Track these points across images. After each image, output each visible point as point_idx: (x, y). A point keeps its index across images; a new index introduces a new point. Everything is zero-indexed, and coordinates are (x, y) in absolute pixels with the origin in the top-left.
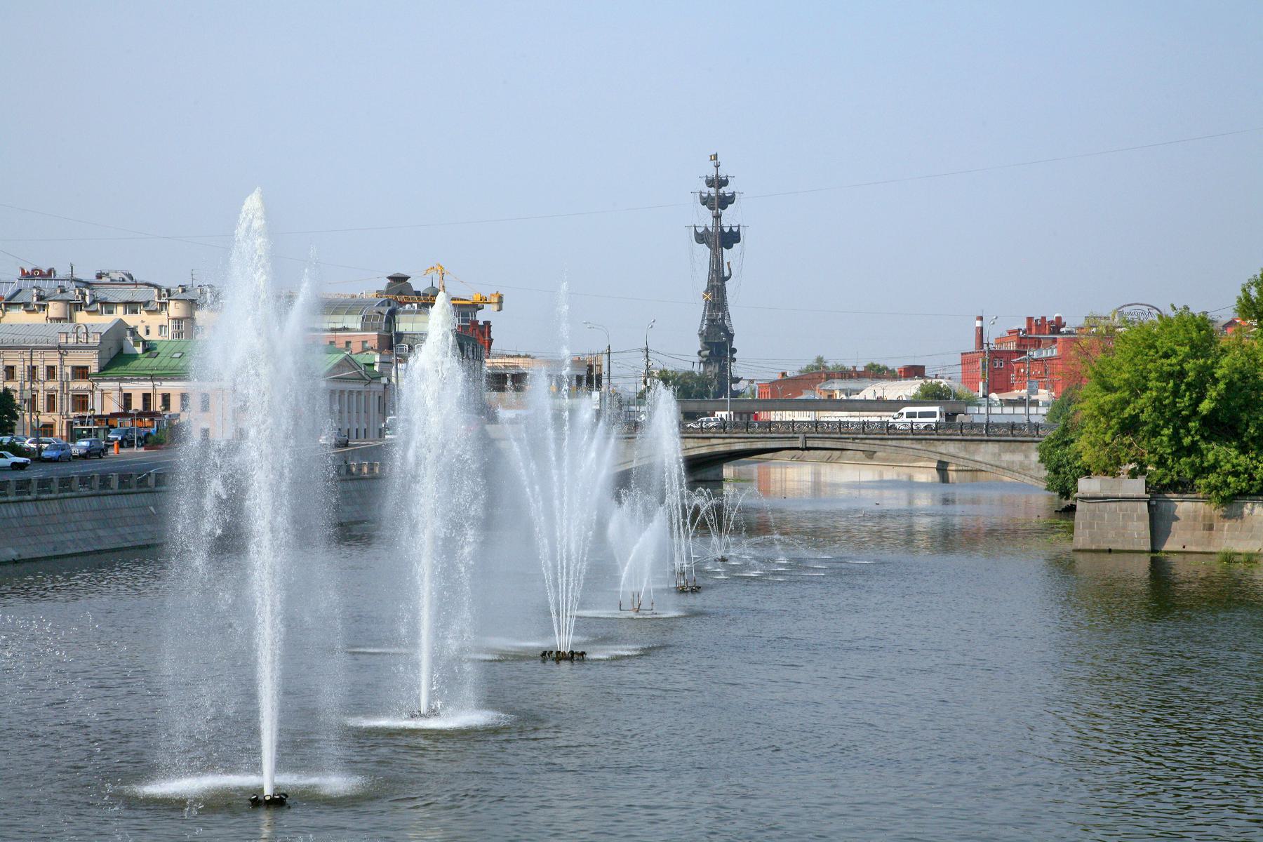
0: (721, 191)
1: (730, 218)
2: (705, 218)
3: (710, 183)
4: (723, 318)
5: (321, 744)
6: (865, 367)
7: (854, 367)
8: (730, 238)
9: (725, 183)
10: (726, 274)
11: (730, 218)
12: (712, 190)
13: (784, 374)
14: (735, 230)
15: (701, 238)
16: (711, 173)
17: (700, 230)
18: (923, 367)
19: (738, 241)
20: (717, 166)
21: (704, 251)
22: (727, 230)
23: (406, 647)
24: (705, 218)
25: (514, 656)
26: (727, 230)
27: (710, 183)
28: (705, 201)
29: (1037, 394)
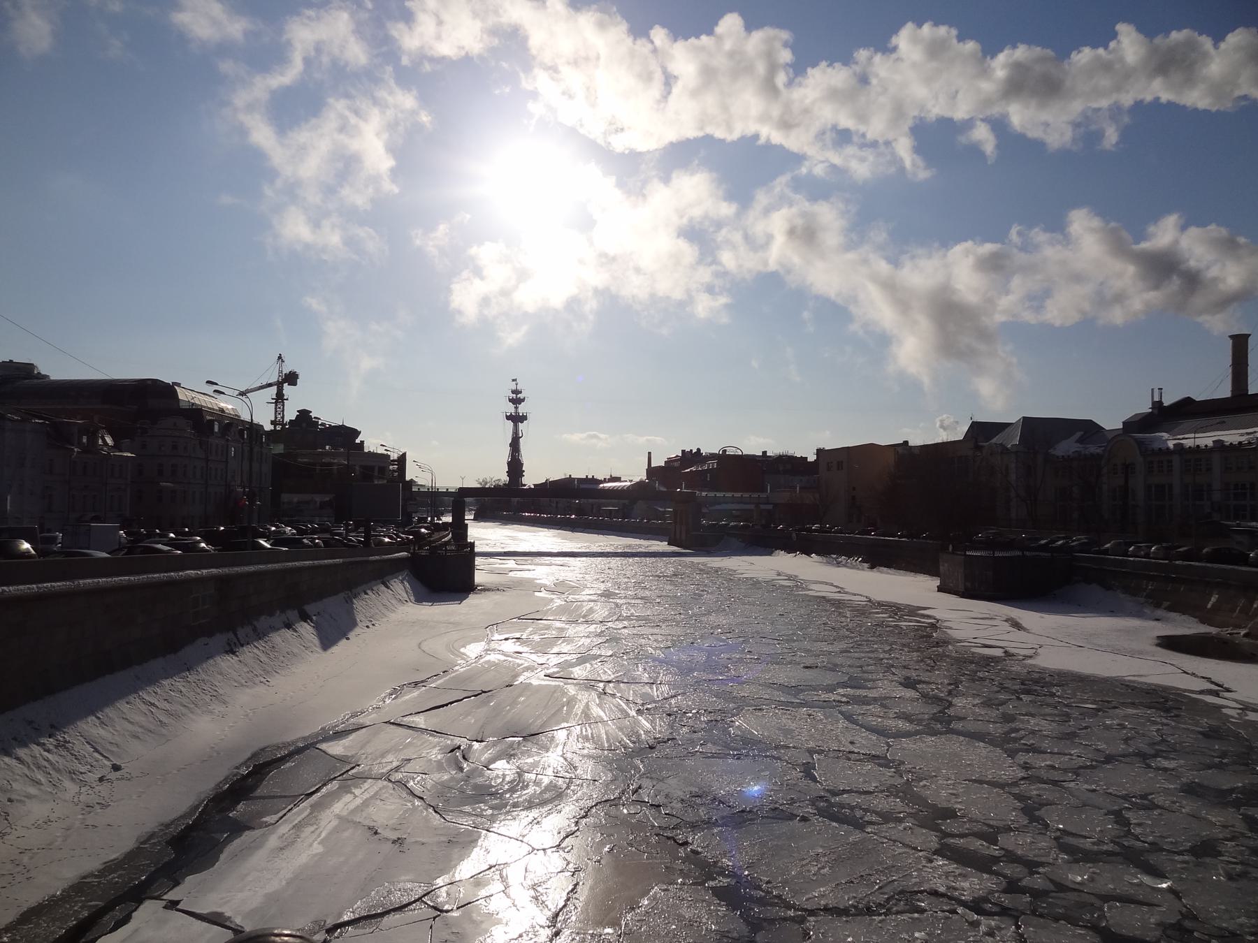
0: (518, 396)
1: (522, 409)
2: (510, 409)
3: (513, 392)
4: (519, 456)
5: (946, 681)
6: (820, 452)
7: (587, 476)
8: (523, 418)
9: (521, 392)
10: (520, 435)
11: (522, 409)
12: (514, 395)
13: (447, 489)
14: (525, 414)
15: (508, 418)
16: (514, 388)
17: (508, 414)
18: (620, 478)
19: (526, 420)
20: (517, 384)
21: (510, 424)
22: (521, 414)
23: (842, 609)
24: (510, 409)
25: (879, 603)
26: (521, 414)
27: (513, 392)
28: (511, 400)
29: (1078, 441)
